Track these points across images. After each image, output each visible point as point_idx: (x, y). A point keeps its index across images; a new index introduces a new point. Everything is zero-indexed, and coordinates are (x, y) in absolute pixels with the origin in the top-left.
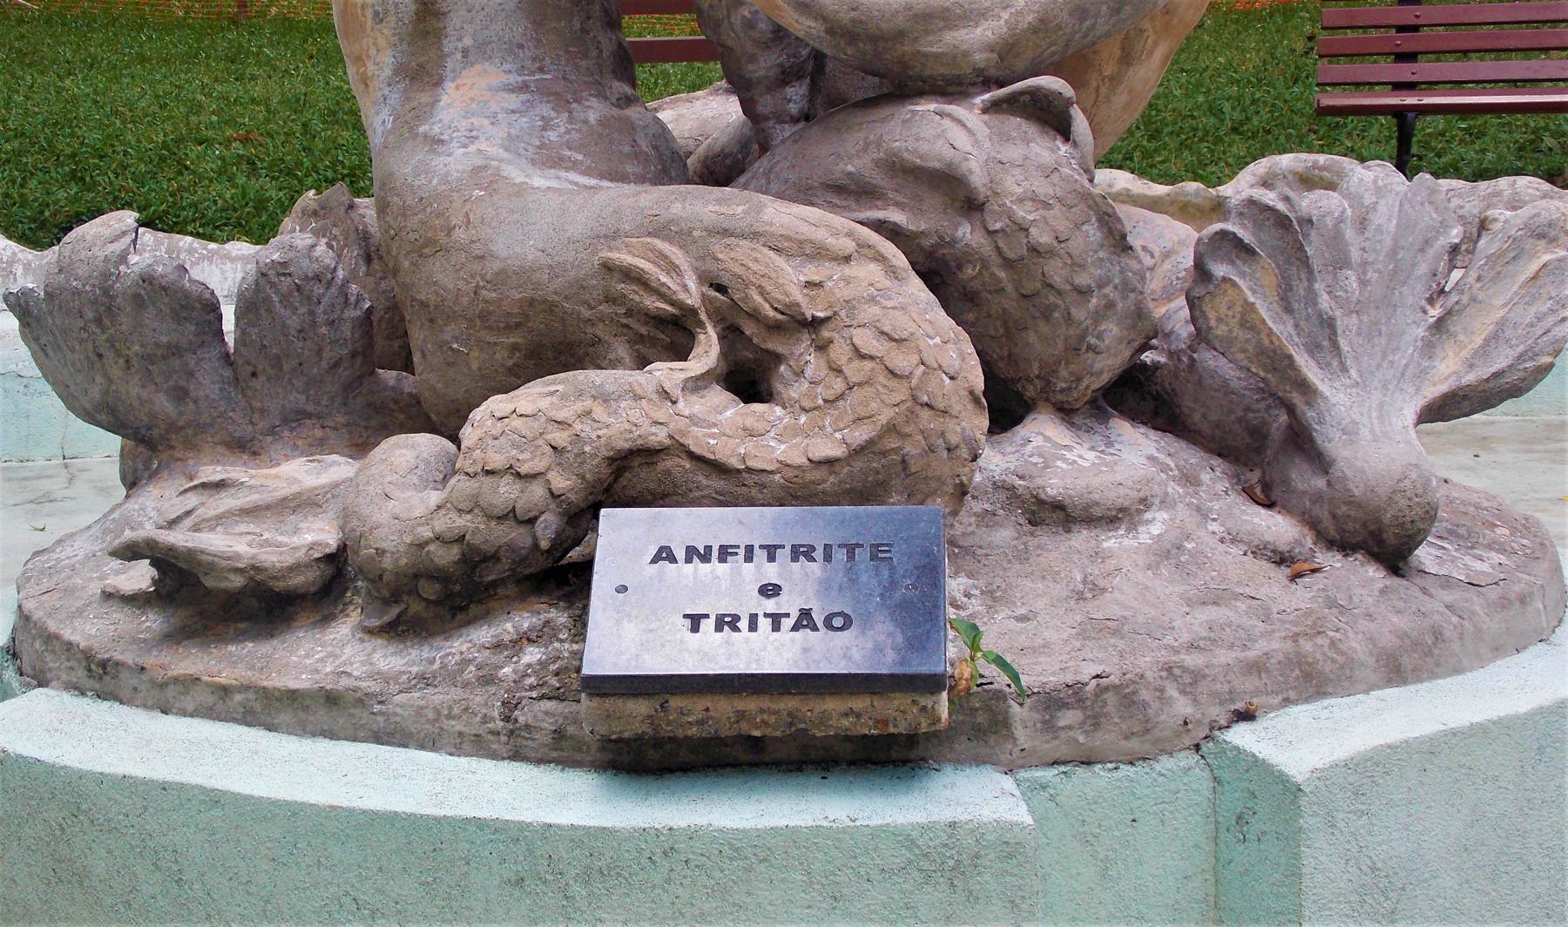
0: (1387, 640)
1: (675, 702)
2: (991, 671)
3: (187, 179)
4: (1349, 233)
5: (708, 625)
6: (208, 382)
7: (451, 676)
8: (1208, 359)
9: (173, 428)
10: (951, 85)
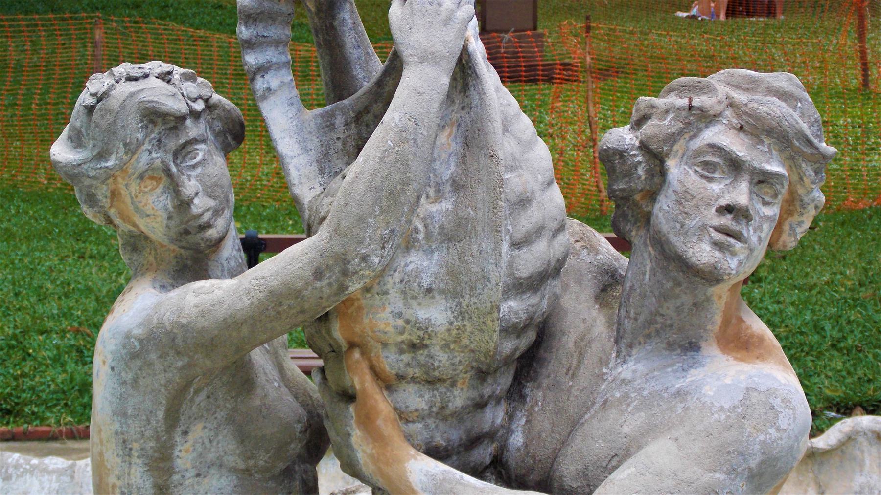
3: (30, 363)
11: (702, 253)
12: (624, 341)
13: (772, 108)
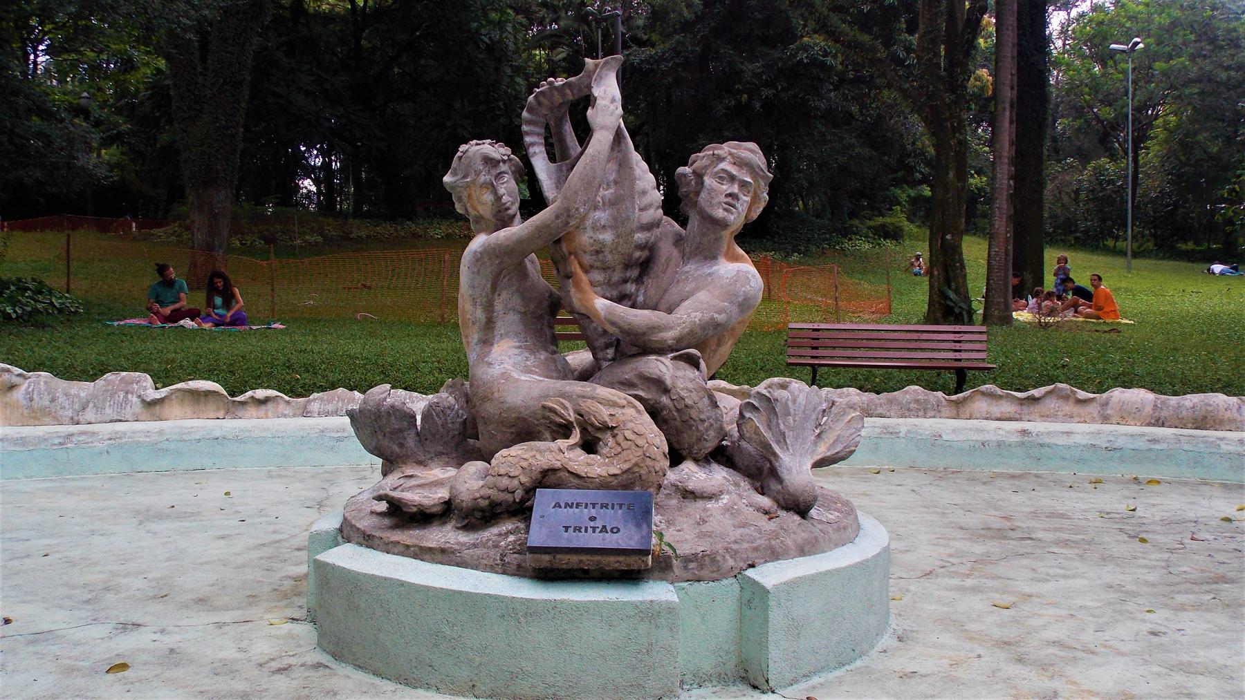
0: (800, 541)
1: (559, 556)
2: (666, 548)
4: (790, 404)
5: (571, 530)
6: (411, 441)
7: (484, 545)
8: (744, 444)
9: (398, 456)
10: (660, 351)
11: (720, 213)
12: (685, 257)
13: (745, 154)
